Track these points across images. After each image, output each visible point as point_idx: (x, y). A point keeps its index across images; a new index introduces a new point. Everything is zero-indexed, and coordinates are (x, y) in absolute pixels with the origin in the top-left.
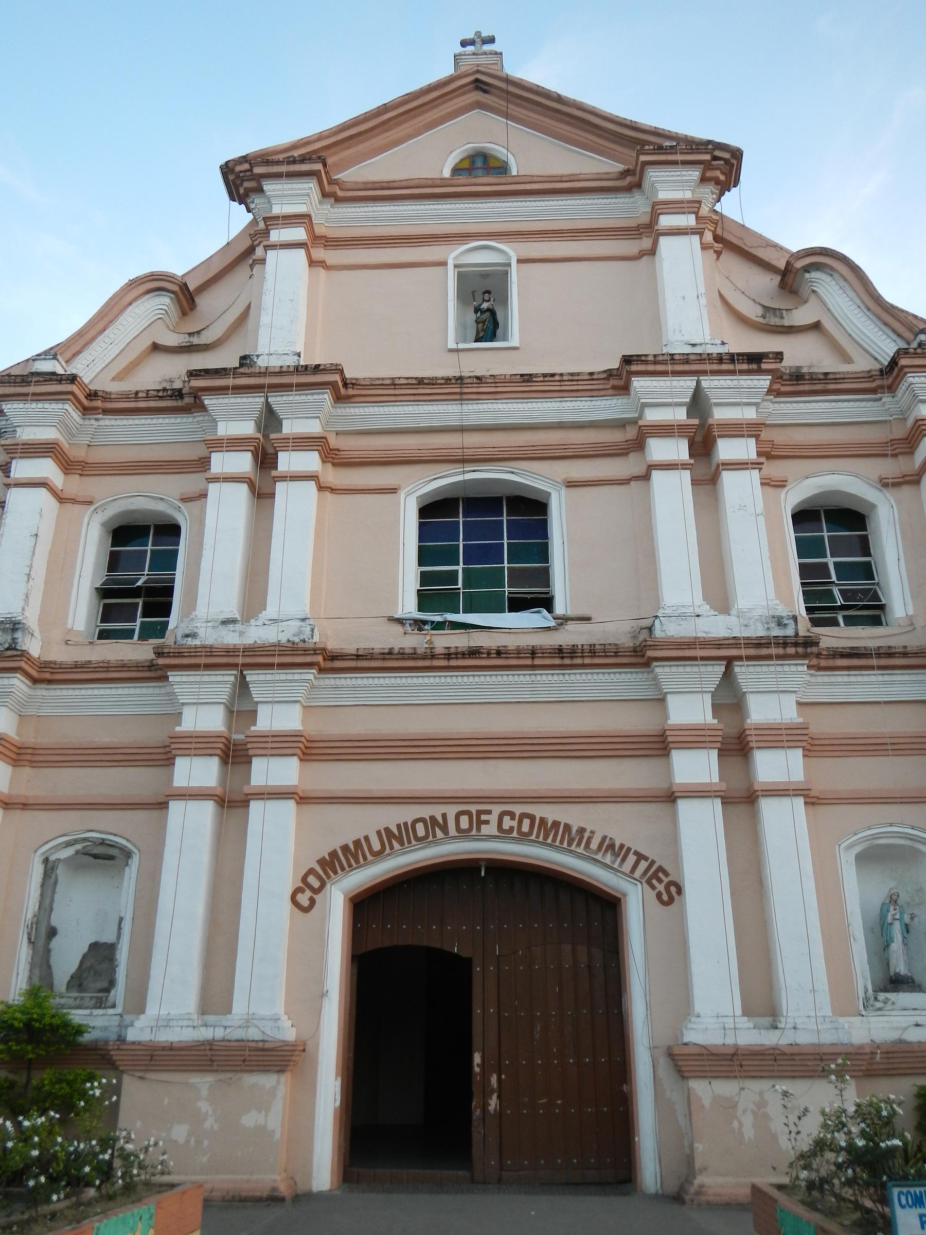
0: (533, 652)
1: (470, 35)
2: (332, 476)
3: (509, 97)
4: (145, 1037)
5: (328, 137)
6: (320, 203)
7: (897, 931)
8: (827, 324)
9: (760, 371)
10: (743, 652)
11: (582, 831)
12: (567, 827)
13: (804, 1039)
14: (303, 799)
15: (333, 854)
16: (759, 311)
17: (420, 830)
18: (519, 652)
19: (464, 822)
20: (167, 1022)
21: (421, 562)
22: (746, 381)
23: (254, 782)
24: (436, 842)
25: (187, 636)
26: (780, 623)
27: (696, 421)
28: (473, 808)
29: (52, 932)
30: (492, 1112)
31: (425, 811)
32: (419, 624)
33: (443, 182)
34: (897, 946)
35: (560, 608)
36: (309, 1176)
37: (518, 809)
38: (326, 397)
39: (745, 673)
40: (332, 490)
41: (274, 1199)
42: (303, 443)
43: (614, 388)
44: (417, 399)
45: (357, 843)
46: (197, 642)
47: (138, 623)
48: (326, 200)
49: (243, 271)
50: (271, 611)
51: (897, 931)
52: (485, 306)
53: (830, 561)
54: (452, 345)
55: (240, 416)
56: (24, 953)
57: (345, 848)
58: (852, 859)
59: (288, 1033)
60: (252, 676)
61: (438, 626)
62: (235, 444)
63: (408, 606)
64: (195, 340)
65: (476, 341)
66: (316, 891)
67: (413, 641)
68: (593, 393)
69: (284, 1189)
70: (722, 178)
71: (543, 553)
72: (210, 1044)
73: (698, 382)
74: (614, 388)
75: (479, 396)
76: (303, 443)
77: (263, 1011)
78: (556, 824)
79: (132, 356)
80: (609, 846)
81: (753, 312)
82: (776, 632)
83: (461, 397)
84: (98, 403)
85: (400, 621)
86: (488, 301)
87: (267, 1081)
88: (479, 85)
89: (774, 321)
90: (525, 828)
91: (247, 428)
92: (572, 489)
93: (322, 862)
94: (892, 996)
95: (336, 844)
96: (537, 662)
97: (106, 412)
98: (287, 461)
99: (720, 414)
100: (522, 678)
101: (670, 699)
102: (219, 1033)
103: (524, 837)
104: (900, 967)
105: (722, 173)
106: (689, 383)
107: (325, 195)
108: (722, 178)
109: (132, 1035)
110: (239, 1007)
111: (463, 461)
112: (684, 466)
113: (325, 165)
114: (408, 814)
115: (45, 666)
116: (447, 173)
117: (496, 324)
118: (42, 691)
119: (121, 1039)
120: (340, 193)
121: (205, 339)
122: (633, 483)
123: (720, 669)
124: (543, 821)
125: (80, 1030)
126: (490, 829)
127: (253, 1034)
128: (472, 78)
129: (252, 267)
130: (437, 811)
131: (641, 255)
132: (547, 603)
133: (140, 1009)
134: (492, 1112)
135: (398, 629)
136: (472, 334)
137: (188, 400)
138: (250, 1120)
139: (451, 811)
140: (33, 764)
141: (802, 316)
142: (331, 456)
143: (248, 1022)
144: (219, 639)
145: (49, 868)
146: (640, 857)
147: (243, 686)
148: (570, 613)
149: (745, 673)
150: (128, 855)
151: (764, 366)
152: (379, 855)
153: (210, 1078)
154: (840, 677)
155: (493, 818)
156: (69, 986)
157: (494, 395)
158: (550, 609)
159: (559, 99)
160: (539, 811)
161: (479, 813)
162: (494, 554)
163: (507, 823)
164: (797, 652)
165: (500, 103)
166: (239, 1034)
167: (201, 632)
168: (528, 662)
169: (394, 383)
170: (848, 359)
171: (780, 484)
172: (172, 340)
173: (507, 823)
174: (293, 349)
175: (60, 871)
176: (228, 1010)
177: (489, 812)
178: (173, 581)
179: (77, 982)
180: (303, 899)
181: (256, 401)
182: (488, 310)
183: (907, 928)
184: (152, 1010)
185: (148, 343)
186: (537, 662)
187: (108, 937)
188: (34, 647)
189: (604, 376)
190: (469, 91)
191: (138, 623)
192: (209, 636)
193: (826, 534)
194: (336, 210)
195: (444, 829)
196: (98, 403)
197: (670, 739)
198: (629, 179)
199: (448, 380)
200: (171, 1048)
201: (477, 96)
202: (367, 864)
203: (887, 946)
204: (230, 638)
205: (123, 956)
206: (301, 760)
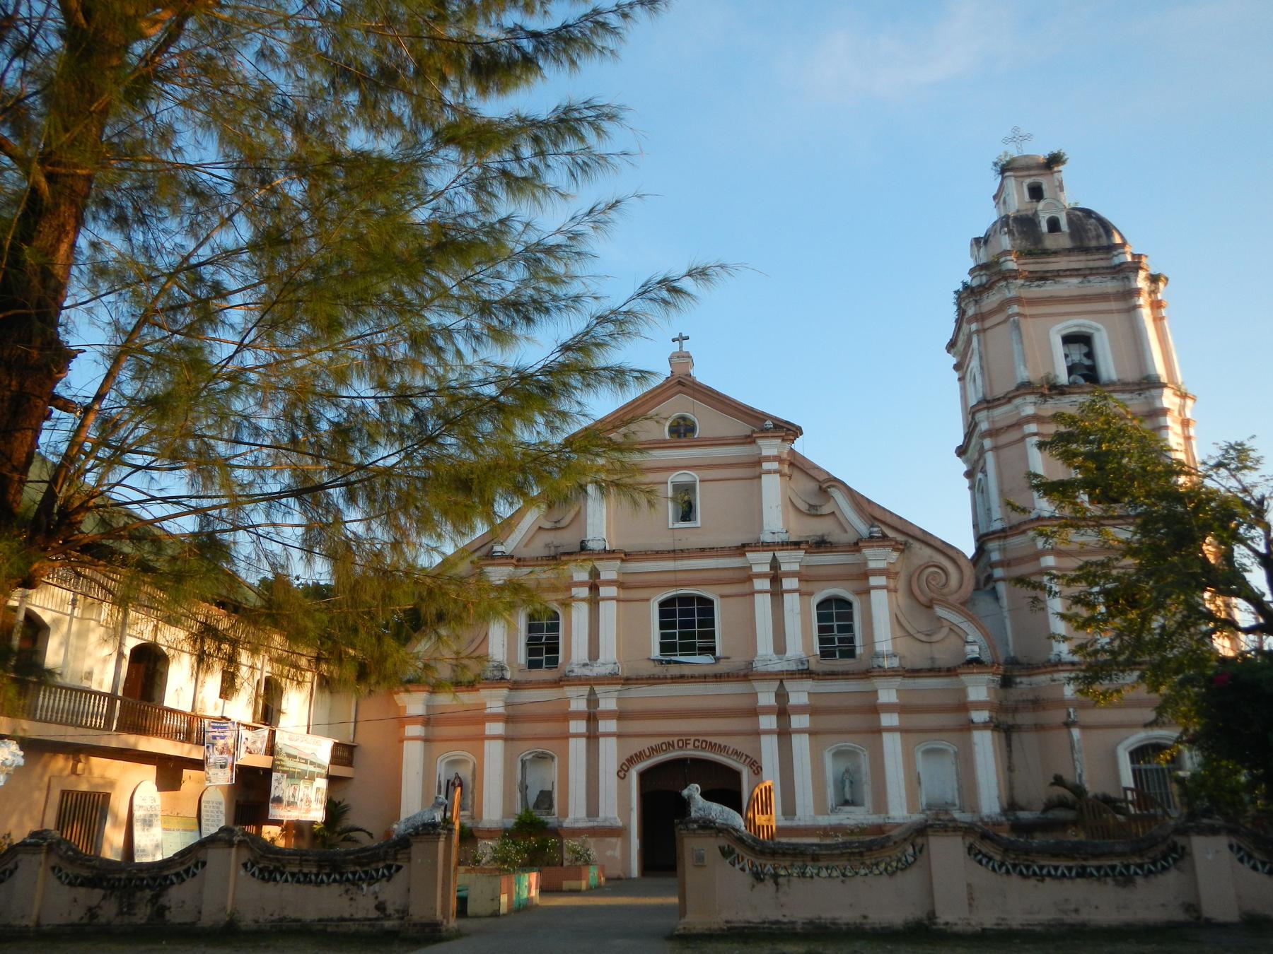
0: (705, 677)
1: (677, 336)
2: (624, 594)
3: (694, 390)
4: (570, 825)
7: (847, 783)
8: (837, 513)
9: (799, 549)
11: (725, 747)
12: (720, 746)
13: (802, 823)
15: (632, 757)
16: (807, 507)
17: (664, 747)
18: (700, 677)
19: (681, 744)
20: (576, 820)
21: (661, 629)
22: (794, 553)
24: (670, 752)
26: (802, 663)
28: (684, 738)
29: (527, 787)
30: (259, 603)
31: (666, 740)
32: (661, 662)
33: (665, 441)
34: (847, 789)
35: (718, 654)
36: (630, 873)
37: (701, 738)
39: (789, 685)
40: (623, 601)
41: (619, 879)
42: (610, 583)
44: (655, 559)
45: (640, 753)
50: (601, 659)
51: (847, 783)
53: (835, 624)
54: (671, 526)
56: (519, 795)
57: (636, 755)
58: (830, 754)
59: (620, 823)
60: (596, 688)
61: (669, 662)
62: (581, 584)
63: (656, 652)
64: (558, 525)
66: (627, 771)
67: (658, 670)
68: (730, 556)
69: (622, 875)
71: (712, 624)
72: (593, 828)
75: (683, 558)
76: (610, 583)
77: (610, 816)
78: (715, 744)
79: (531, 534)
80: (736, 753)
81: (804, 507)
82: (801, 667)
83: (675, 559)
85: (654, 660)
87: (614, 840)
88: (680, 383)
89: (813, 512)
90: (704, 745)
92: (724, 599)
93: (627, 760)
94: (842, 808)
95: (633, 753)
98: (604, 591)
99: (784, 568)
100: (702, 686)
101: (759, 695)
102: (596, 824)
103: (703, 749)
104: (848, 797)
106: (770, 554)
109: (565, 825)
110: (602, 815)
111: (676, 586)
112: (766, 592)
114: (659, 741)
115: (515, 682)
118: (513, 693)
119: (561, 826)
121: (563, 524)
123: (778, 683)
124: (710, 743)
125: (547, 823)
126: (690, 746)
127: (607, 824)
130: (670, 739)
132: (711, 650)
133: (566, 816)
134: (259, 603)
135: (652, 664)
138: (609, 853)
139: (676, 740)
140: (513, 722)
141: (826, 509)
142: (621, 585)
143: (606, 820)
145: (524, 763)
146: (747, 756)
147: (592, 693)
148: (722, 655)
149: (789, 685)
150: (553, 758)
152: (649, 757)
153: (594, 839)
154: (828, 683)
155: (692, 742)
156: (534, 807)
157: (689, 558)
158: (714, 654)
159: (718, 393)
160: (709, 739)
162: (691, 613)
163: (697, 744)
165: (691, 392)
166: (601, 824)
167: (576, 670)
169: (646, 553)
170: (846, 531)
171: (811, 594)
172: (548, 525)
173: (697, 744)
175: (528, 764)
176: (598, 816)
178: (557, 638)
179: (537, 806)
180: (622, 774)
183: (851, 782)
184: (571, 816)
187: (548, 788)
188: (508, 675)
192: (578, 671)
193: (834, 611)
195: (673, 746)
199: (669, 552)
200: (579, 829)
201: (680, 387)
202: (644, 760)
203: (844, 788)
204: (586, 672)
205: (556, 796)
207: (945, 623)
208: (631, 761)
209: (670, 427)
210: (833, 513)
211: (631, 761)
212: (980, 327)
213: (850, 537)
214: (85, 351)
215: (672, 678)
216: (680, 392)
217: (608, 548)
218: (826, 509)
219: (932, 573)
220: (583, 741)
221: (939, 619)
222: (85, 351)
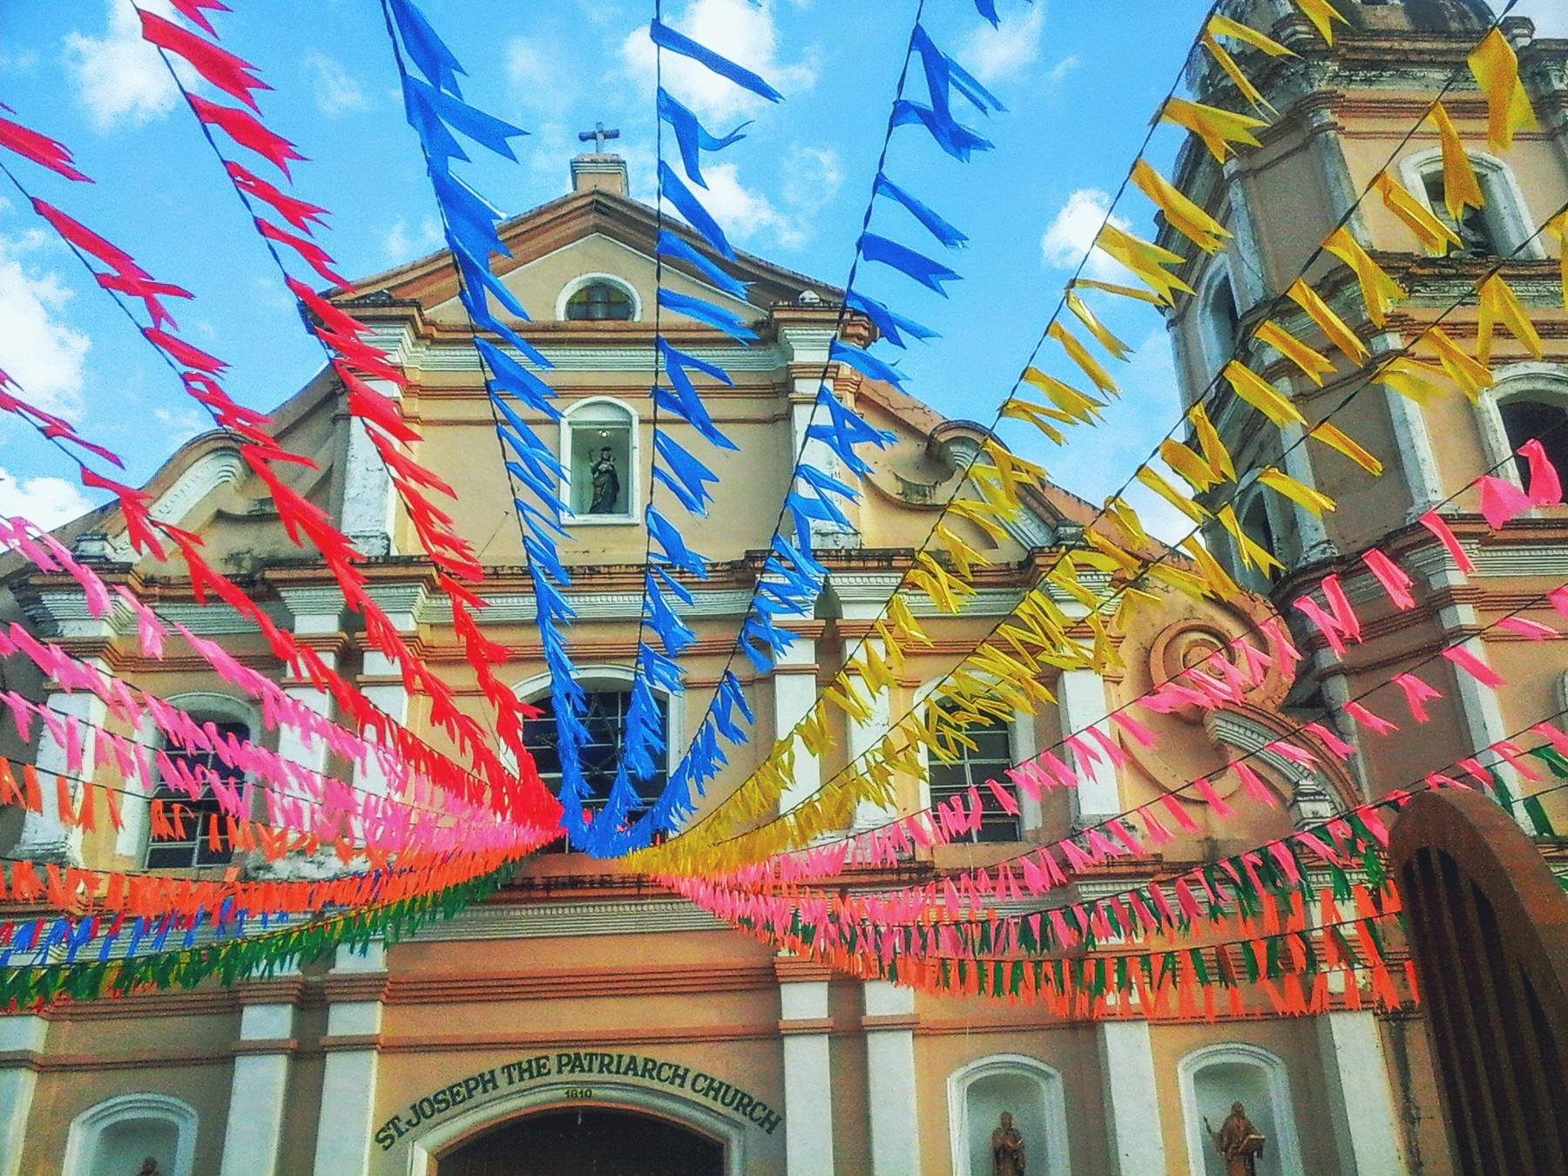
5: (423, 266)
6: (414, 345)
9: (891, 569)
10: (855, 879)
14: (388, 1048)
16: (900, 487)
22: (875, 579)
23: (331, 1033)
25: (259, 868)
27: (822, 623)
28: (571, 1052)
33: (555, 328)
38: (422, 591)
43: (737, 581)
46: (270, 876)
47: (198, 841)
48: (421, 342)
49: (319, 426)
52: (603, 467)
55: (316, 610)
65: (593, 511)
70: (865, 333)
73: (826, 578)
74: (737, 581)
81: (891, 488)
84: (157, 591)
86: (608, 460)
89: (916, 500)
91: (327, 625)
96: (643, 891)
97: (163, 599)
99: (850, 614)
105: (865, 328)
107: (419, 337)
108: (865, 333)
113: (419, 310)
116: (561, 315)
117: (615, 486)
120: (436, 335)
122: (756, 686)
128: (589, 199)
129: (334, 420)
131: (773, 420)
136: (588, 507)
137: (260, 588)
144: (296, 872)
151: (894, 564)
157: (610, 588)
160: (659, 1054)
161: (538, 1060)
164: (911, 878)
168: (635, 891)
170: (992, 544)
172: (240, 507)
174: (381, 529)
177: (547, 1058)
181: (336, 596)
182: (607, 471)
185: (213, 511)
186: (643, 891)
189: (727, 567)
190: (588, 213)
191: (198, 841)
194: (432, 353)
196: (157, 591)
197: (779, 973)
198: (763, 332)
201: (593, 219)
205: (1242, 37)
206: (384, 1004)
207: (1234, 755)
208: (426, 1110)
209: (570, 304)
210: (1013, 469)
211: (426, 1110)
212: (1247, 167)
213: (1008, 553)
214: (453, 740)
215: (547, 887)
216: (598, 229)
217: (394, 552)
218: (942, 495)
219: (1195, 643)
220: (278, 1067)
221: (1220, 748)
222: (453, 740)
